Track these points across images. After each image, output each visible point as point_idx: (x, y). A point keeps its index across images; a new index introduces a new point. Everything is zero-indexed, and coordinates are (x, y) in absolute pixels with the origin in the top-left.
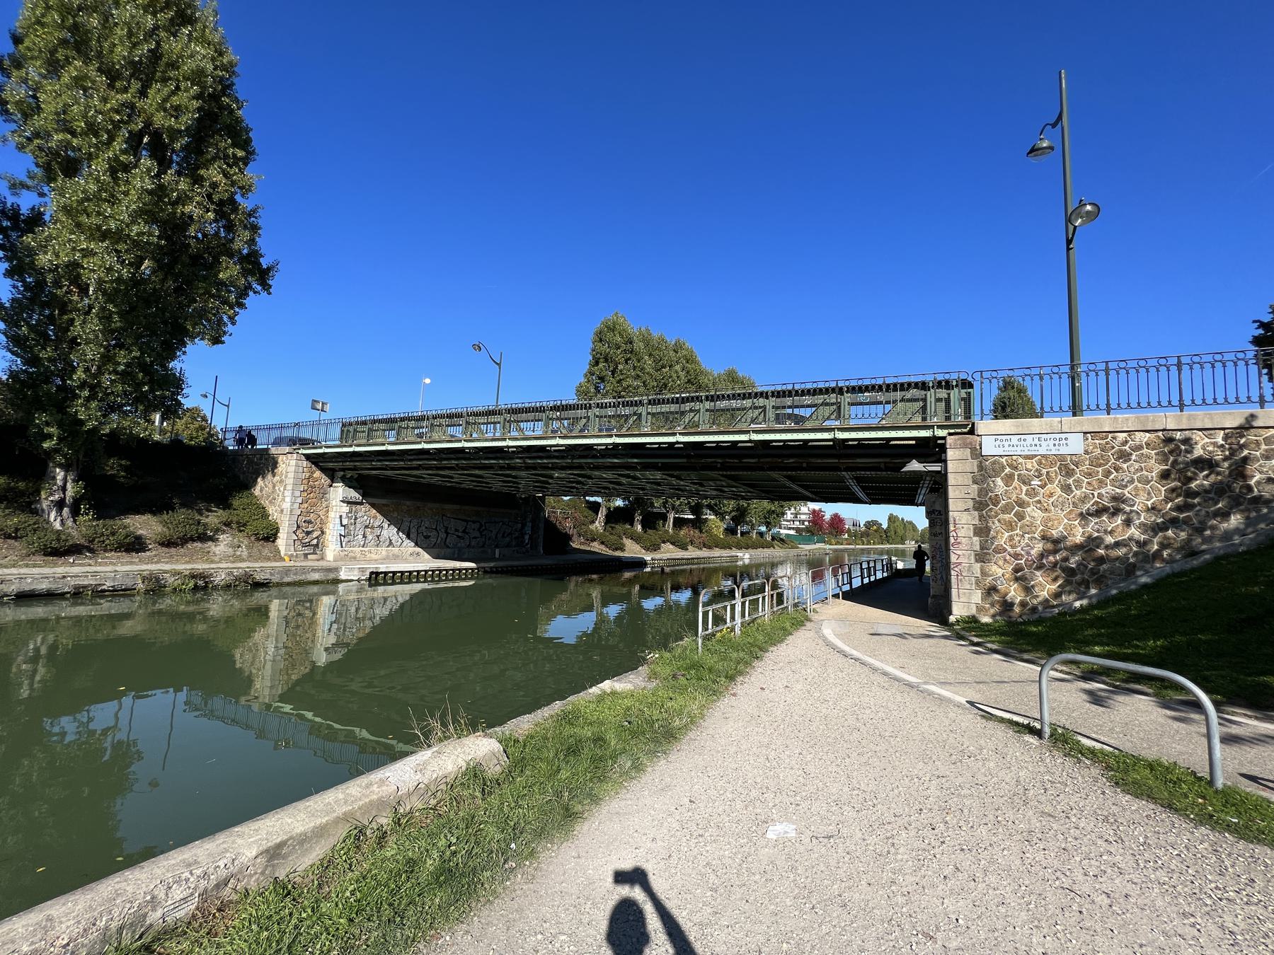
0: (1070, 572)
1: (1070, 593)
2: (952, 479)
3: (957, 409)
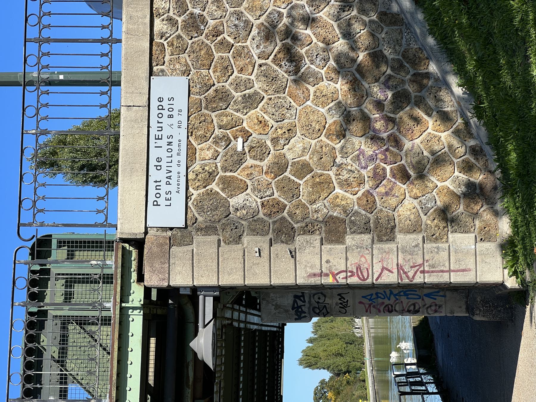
0: (401, 99)
1: (438, 100)
2: (232, 278)
3: (92, 262)
